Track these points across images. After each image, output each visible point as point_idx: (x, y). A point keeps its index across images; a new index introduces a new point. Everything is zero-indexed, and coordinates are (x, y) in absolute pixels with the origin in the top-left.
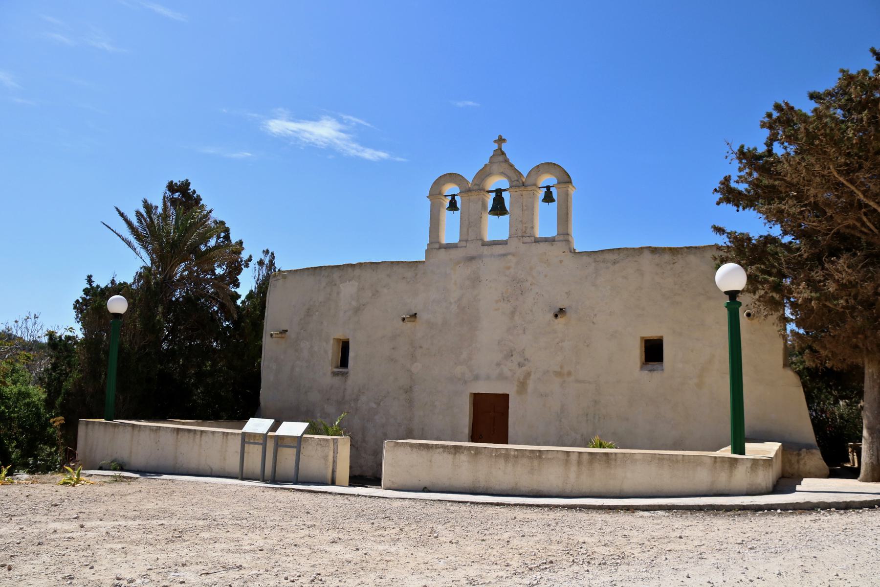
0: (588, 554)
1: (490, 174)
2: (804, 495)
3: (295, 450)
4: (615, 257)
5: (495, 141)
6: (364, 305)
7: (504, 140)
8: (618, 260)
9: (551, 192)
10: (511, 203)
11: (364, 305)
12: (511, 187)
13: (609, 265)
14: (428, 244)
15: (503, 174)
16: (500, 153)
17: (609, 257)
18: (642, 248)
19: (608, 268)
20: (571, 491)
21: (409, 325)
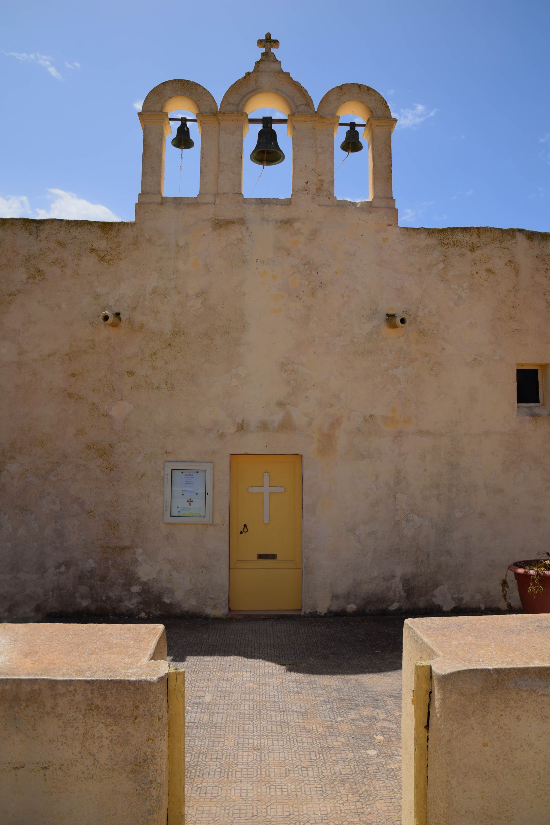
0: (498, 706)
1: (256, 90)
2: (72, 626)
3: (211, 522)
4: (474, 238)
5: (260, 42)
6: (10, 295)
7: (276, 42)
8: (478, 244)
9: (357, 133)
10: (94, 199)
11: (10, 295)
12: (292, 115)
13: (465, 250)
14: (139, 194)
15: (278, 92)
16: (267, 57)
17: (461, 237)
18: (512, 233)
19: (463, 255)
20: (214, 615)
21: (106, 332)
